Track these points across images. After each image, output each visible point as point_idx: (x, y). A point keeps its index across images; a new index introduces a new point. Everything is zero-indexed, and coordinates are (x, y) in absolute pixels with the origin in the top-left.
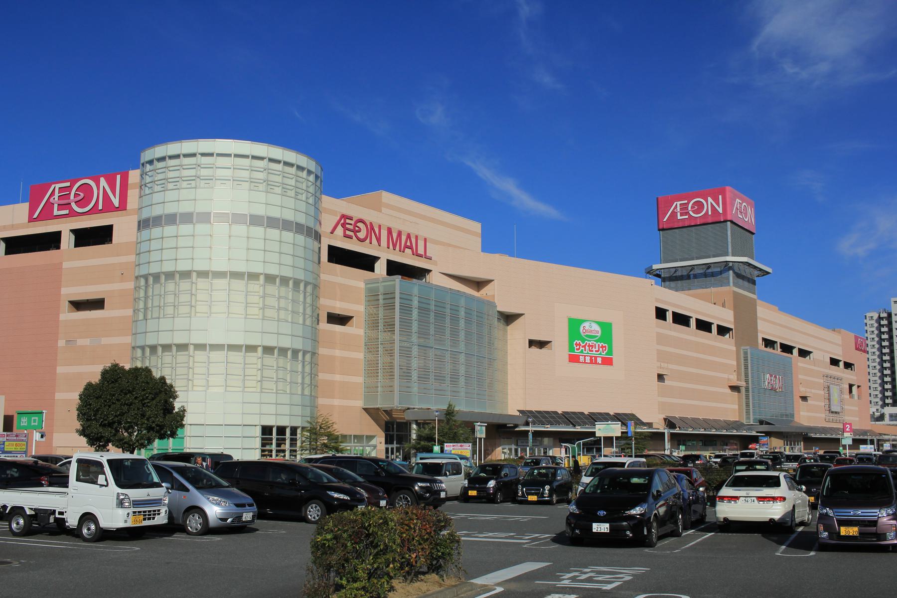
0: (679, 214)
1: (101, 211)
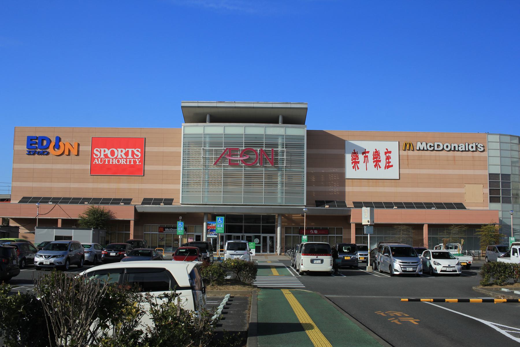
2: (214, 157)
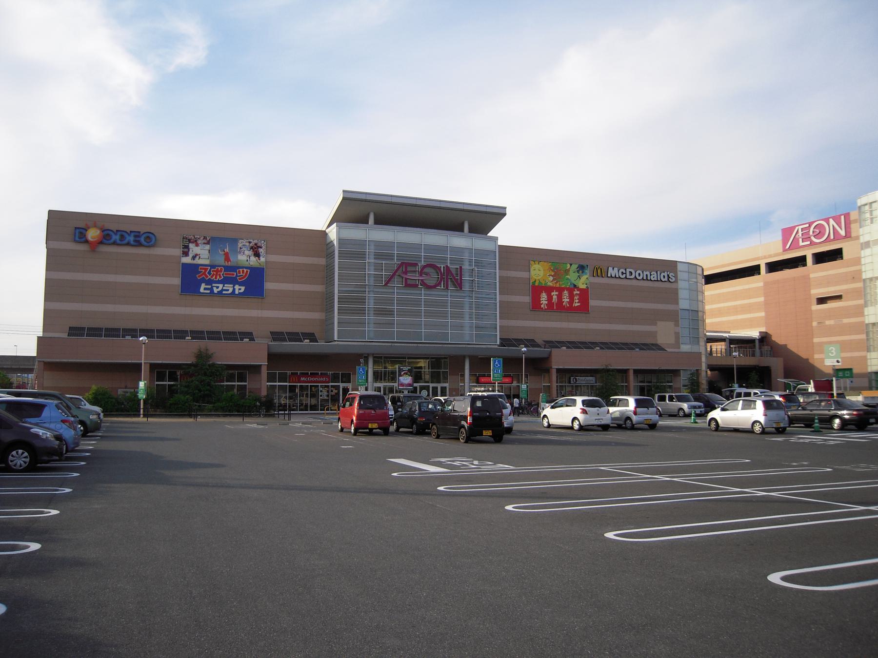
1: (832, 240)
2: (384, 273)
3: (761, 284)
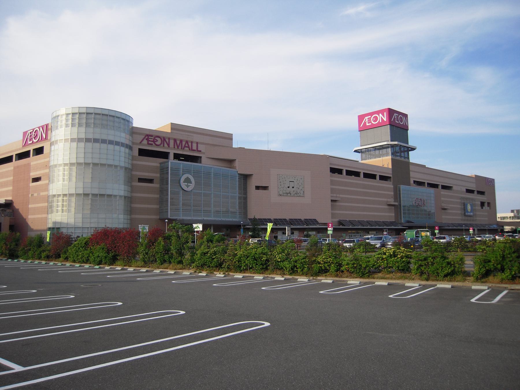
0: (367, 123)
3: (12, 168)
